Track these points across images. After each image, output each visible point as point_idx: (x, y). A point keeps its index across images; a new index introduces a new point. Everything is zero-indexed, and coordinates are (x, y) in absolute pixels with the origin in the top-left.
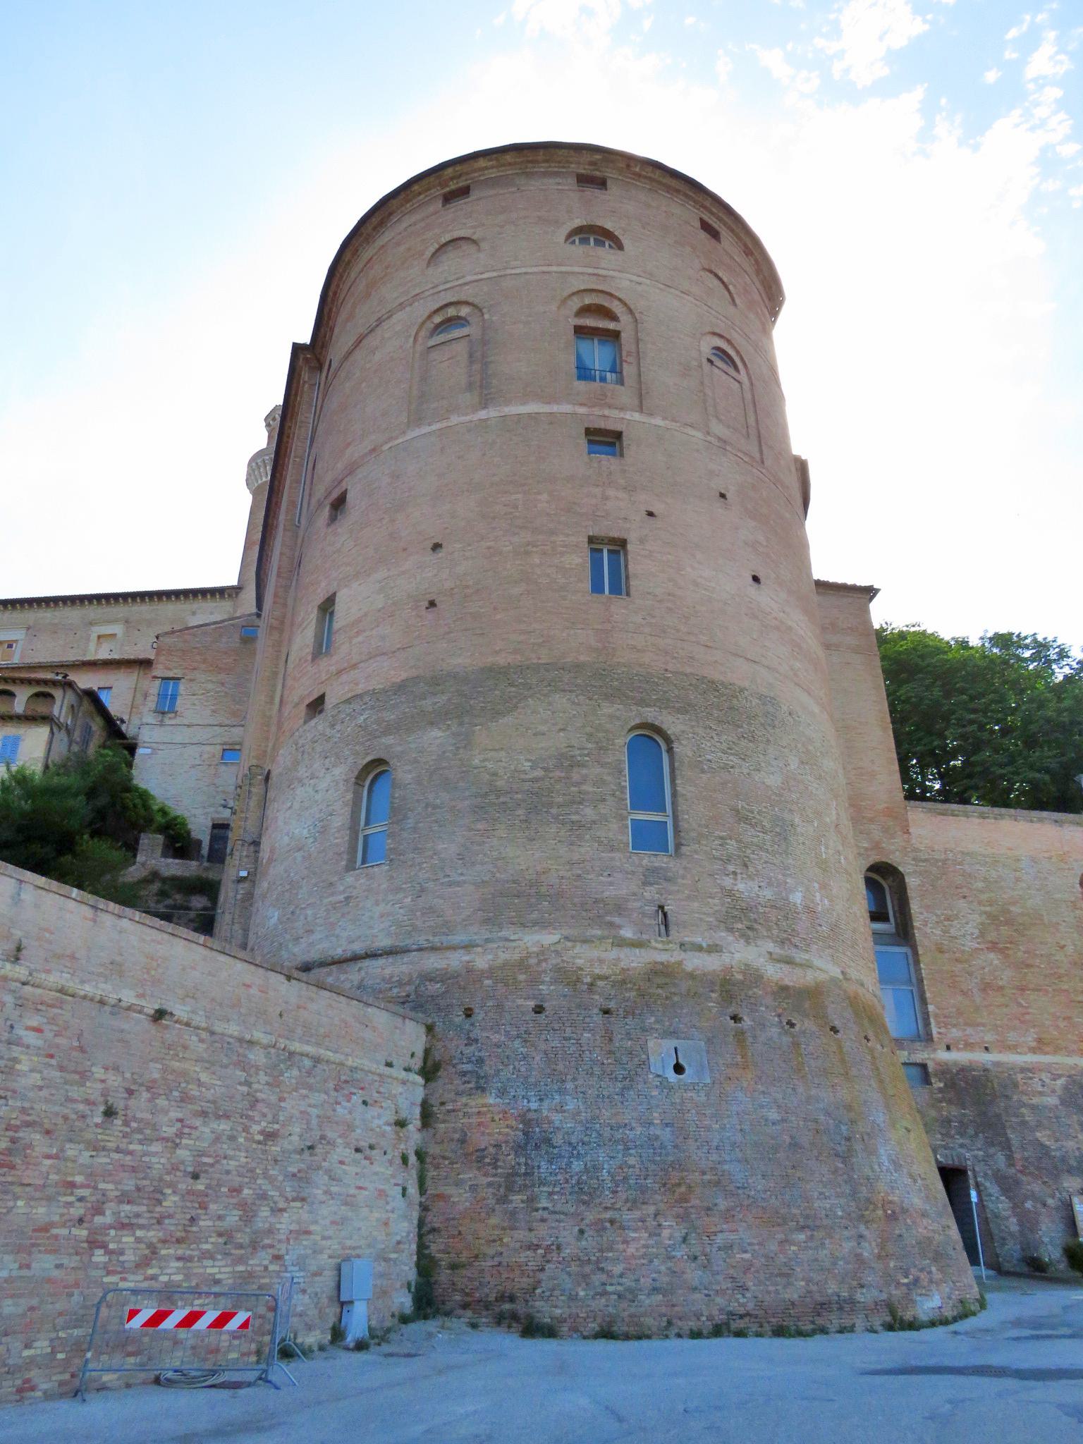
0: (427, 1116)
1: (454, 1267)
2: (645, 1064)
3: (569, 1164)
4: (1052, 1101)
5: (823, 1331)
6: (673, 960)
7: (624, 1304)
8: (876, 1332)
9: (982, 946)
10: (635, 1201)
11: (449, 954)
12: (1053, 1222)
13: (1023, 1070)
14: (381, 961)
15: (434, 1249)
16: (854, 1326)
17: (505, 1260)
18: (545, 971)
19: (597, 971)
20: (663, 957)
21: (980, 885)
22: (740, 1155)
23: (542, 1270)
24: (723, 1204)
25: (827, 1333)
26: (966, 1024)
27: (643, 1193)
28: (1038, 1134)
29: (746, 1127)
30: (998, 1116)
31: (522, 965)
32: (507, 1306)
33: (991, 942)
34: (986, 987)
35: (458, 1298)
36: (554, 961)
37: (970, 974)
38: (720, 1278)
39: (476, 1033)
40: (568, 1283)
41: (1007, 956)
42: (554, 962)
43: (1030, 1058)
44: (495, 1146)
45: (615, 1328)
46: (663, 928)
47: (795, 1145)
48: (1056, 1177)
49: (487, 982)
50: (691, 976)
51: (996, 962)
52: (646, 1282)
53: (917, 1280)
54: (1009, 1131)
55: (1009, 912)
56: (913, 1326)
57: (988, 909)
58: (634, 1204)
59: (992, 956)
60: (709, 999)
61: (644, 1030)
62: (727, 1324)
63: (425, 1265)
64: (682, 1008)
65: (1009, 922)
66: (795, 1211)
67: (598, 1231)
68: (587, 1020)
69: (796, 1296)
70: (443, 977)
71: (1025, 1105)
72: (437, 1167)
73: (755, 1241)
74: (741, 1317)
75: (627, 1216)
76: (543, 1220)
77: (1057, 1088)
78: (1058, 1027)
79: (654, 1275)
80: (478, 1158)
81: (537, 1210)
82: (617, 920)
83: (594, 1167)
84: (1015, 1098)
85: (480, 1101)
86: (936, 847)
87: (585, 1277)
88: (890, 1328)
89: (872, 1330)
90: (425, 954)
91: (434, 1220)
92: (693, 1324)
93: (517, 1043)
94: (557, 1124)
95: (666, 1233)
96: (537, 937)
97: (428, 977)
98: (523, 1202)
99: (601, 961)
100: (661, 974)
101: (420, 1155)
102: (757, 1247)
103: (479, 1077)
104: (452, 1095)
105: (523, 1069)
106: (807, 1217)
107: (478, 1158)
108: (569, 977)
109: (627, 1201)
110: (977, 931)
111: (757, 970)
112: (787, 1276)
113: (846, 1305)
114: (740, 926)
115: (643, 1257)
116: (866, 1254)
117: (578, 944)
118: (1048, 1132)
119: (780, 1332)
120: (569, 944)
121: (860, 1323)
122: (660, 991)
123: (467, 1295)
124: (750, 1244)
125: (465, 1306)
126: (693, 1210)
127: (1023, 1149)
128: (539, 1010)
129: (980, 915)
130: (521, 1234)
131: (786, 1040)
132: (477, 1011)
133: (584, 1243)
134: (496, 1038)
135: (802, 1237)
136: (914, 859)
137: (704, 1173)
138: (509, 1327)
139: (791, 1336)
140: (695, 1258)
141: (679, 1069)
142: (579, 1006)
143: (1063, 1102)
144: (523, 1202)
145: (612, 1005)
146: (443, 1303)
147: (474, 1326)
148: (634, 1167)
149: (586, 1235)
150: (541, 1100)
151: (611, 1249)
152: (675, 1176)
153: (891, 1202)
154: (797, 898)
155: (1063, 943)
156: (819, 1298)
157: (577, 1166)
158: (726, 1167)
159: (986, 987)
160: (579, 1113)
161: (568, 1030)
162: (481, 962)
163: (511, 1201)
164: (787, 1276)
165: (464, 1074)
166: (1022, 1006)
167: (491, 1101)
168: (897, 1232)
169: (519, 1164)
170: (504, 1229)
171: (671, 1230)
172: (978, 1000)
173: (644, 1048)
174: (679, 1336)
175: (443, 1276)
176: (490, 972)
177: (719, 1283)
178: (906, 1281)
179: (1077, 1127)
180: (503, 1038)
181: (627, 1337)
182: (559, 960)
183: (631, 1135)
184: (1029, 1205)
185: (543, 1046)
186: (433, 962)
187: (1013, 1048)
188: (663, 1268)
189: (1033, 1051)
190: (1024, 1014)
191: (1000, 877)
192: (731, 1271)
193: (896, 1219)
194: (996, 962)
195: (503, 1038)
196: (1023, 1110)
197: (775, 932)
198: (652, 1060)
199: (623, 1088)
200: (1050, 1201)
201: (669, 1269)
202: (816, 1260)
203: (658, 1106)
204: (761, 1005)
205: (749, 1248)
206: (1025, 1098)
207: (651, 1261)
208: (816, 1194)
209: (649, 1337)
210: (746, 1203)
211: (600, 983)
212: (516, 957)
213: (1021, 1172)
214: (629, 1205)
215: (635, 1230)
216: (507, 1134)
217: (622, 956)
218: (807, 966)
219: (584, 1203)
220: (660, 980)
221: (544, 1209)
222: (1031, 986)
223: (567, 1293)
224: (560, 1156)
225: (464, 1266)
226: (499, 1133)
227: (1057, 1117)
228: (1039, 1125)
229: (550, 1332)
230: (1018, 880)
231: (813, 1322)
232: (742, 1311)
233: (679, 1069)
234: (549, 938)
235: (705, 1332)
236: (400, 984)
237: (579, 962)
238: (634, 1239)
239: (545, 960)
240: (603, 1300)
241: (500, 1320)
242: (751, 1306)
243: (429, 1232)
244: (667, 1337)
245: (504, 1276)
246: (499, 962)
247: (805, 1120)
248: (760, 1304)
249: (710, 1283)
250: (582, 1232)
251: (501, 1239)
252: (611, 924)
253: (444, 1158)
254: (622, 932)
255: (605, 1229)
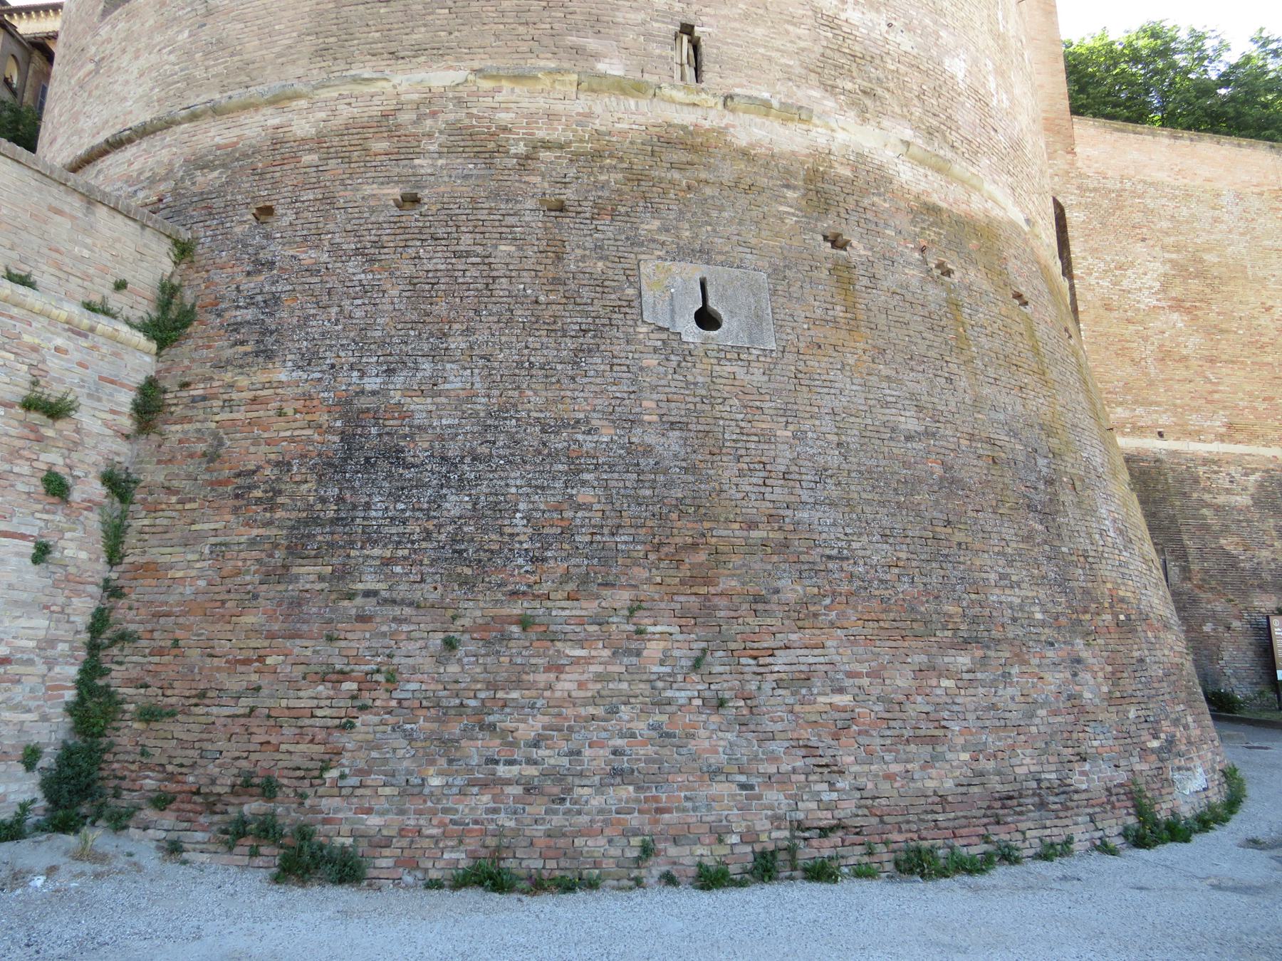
0: (149, 407)
1: (149, 715)
2: (632, 306)
3: (437, 501)
4: (1243, 500)
5: (1008, 856)
6: (707, 124)
7: (538, 809)
8: (1113, 852)
9: (1163, 304)
10: (585, 580)
11: (244, 118)
12: (1238, 649)
13: (1206, 462)
14: (130, 151)
15: (117, 677)
16: (1069, 840)
17: (264, 702)
18: (430, 135)
19: (540, 134)
20: (687, 118)
21: (1165, 224)
22: (835, 493)
23: (348, 726)
24: (792, 590)
25: (1017, 861)
26: (1135, 402)
27: (604, 562)
28: (1223, 541)
29: (852, 439)
30: (1173, 519)
31: (385, 123)
32: (253, 807)
33: (1173, 299)
34: (1164, 356)
35: (149, 783)
36: (452, 114)
37: (1145, 339)
38: (777, 747)
39: (278, 251)
40: (403, 757)
41: (1196, 318)
42: (451, 117)
43: (1216, 448)
44: (277, 464)
45: (510, 864)
46: (690, 72)
47: (951, 483)
48: (1245, 594)
49: (308, 158)
50: (744, 153)
51: (1180, 325)
52: (595, 758)
53: (1171, 741)
54: (1185, 537)
55: (1201, 261)
56: (1176, 832)
57: (1174, 256)
58: (582, 587)
59: (1175, 316)
60: (780, 199)
61: (634, 242)
62: (792, 851)
63: (93, 707)
64: (721, 209)
65: (1201, 275)
66: (950, 609)
67: (487, 643)
68: (510, 220)
69: (949, 784)
70: (231, 159)
71: (1208, 506)
72: (153, 509)
73: (864, 668)
74: (824, 832)
75: (563, 611)
76: (363, 618)
77: (1250, 485)
78: (1255, 409)
79: (619, 742)
80: (242, 490)
81: (351, 596)
82: (592, 43)
83: (494, 507)
84: (1195, 495)
85: (261, 377)
86: (1110, 173)
87: (447, 744)
88: (1139, 841)
89: (1104, 848)
90: (202, 124)
91: (126, 616)
92: (706, 853)
93: (352, 266)
94: (420, 419)
95: (654, 649)
96: (419, 75)
97: (200, 163)
98: (321, 578)
99: (551, 116)
100: (687, 146)
101: (119, 485)
102: (865, 681)
103: (266, 332)
104: (207, 370)
105: (359, 313)
106: (975, 620)
107: (242, 490)
108: (480, 144)
109: (567, 577)
110: (1157, 285)
111: (880, 167)
112: (933, 740)
113: (1054, 797)
114: (849, 86)
115: (593, 701)
116: (1087, 695)
117: (506, 85)
118: (1236, 539)
119: (916, 864)
120: (487, 85)
121: (1082, 837)
122: (676, 175)
123: (171, 777)
124: (850, 675)
125: (161, 802)
126: (722, 602)
127: (1203, 559)
128: (411, 200)
129: (1164, 263)
130: (309, 649)
131: (934, 293)
132: (279, 211)
133: (453, 669)
134: (309, 257)
135: (963, 660)
136: (1079, 188)
137: (752, 525)
138: (254, 853)
139: (943, 873)
140: (721, 703)
141: (706, 319)
142: (494, 195)
143: (1257, 502)
144: (321, 578)
145: (569, 195)
146: (117, 796)
147: (174, 849)
148: (588, 507)
149: (460, 652)
150: (390, 372)
151: (518, 684)
152: (684, 530)
153: (1122, 600)
154: (957, 67)
155: (1269, 303)
156: (995, 784)
157: (455, 504)
158: (803, 515)
159: (1164, 356)
160: (471, 397)
161: (467, 239)
162: (302, 125)
163: (296, 578)
164: (933, 740)
165: (236, 327)
166: (1211, 382)
167: (283, 377)
168: (1136, 654)
169: (323, 500)
170: (271, 636)
171: (665, 642)
172: (1152, 371)
173: (632, 276)
174: (669, 880)
175: (127, 735)
176: (319, 142)
177: (773, 759)
178: (1155, 744)
179: (1274, 533)
180: (325, 257)
181: (538, 885)
182: (462, 114)
183: (588, 442)
184: (1208, 628)
185: (408, 269)
186: (213, 135)
187: (1196, 435)
188: (640, 726)
189: (1221, 438)
190: (1211, 392)
191: (1193, 215)
192: (806, 733)
193: (1133, 631)
194: (1180, 325)
195: (325, 257)
196: (1204, 511)
197: (917, 112)
198: (647, 296)
199: (576, 352)
200: (1236, 624)
201: (652, 727)
202: (993, 707)
203: (654, 388)
204: (887, 225)
205: (848, 682)
206: (1207, 497)
207: (613, 711)
208: (993, 577)
209: (592, 885)
210: (845, 588)
211: (544, 155)
212: (375, 111)
213: (1200, 587)
214: (571, 586)
215: (581, 643)
216: (310, 441)
217: (598, 109)
218: (970, 186)
219: (463, 581)
220: (680, 156)
221: (368, 594)
222: (1224, 357)
223: (401, 779)
224: (421, 485)
225: (172, 714)
226: (292, 439)
227: (1247, 521)
228: (1225, 530)
229: (347, 870)
230: (1216, 220)
231: (986, 839)
232: (826, 819)
233: (706, 319)
234: (442, 77)
235: (734, 869)
236: (153, 181)
237: (504, 117)
238: (576, 661)
239: (434, 114)
240: (486, 798)
241: (235, 834)
242: (847, 808)
243: (113, 642)
244: (638, 882)
245: (258, 738)
246: (339, 122)
247: (972, 437)
248: (867, 801)
249: (755, 758)
250: (450, 644)
251: (261, 659)
252: (578, 51)
253: (169, 490)
254: (601, 67)
255: (505, 638)
